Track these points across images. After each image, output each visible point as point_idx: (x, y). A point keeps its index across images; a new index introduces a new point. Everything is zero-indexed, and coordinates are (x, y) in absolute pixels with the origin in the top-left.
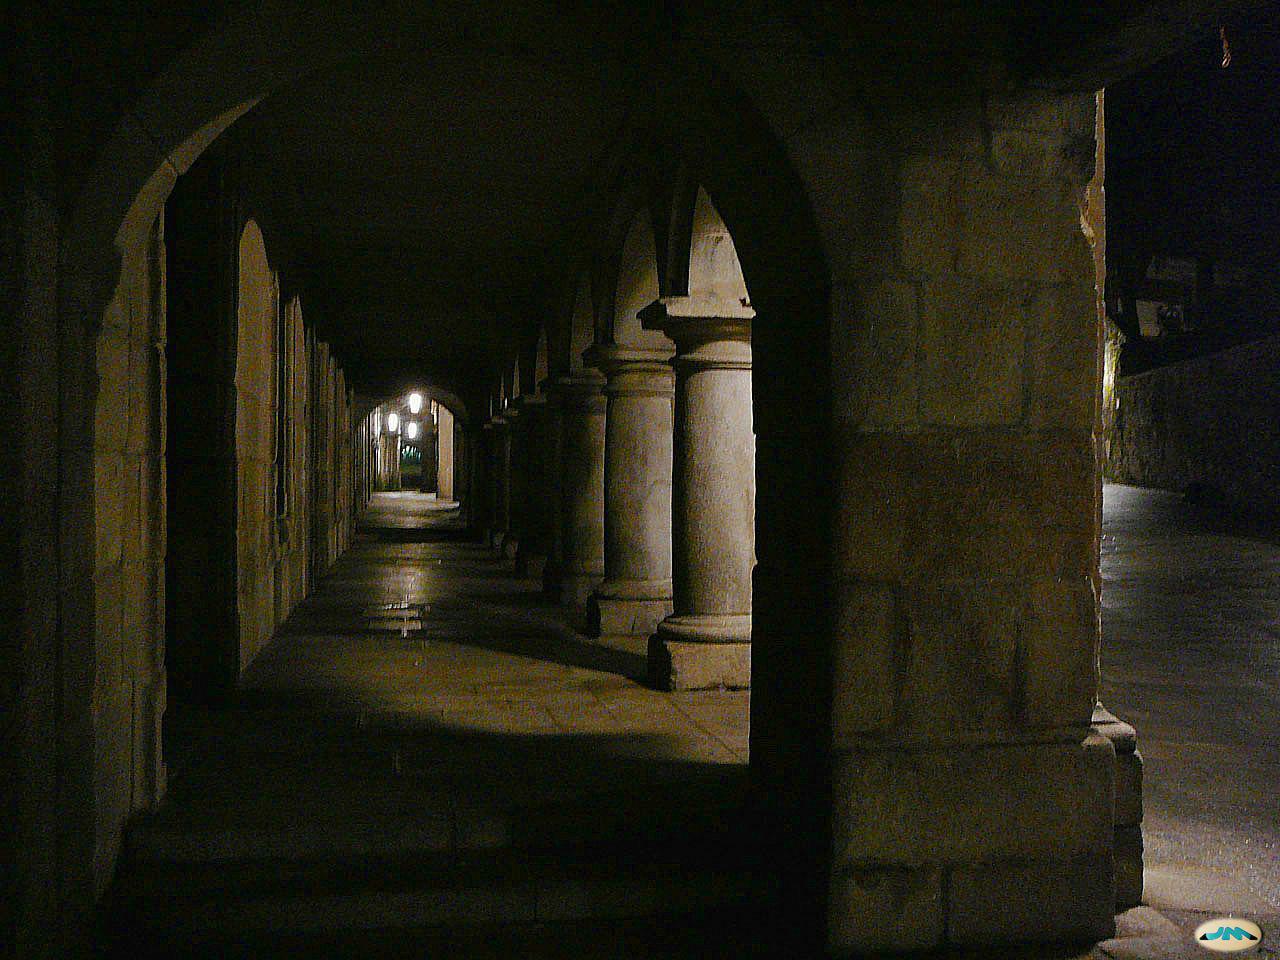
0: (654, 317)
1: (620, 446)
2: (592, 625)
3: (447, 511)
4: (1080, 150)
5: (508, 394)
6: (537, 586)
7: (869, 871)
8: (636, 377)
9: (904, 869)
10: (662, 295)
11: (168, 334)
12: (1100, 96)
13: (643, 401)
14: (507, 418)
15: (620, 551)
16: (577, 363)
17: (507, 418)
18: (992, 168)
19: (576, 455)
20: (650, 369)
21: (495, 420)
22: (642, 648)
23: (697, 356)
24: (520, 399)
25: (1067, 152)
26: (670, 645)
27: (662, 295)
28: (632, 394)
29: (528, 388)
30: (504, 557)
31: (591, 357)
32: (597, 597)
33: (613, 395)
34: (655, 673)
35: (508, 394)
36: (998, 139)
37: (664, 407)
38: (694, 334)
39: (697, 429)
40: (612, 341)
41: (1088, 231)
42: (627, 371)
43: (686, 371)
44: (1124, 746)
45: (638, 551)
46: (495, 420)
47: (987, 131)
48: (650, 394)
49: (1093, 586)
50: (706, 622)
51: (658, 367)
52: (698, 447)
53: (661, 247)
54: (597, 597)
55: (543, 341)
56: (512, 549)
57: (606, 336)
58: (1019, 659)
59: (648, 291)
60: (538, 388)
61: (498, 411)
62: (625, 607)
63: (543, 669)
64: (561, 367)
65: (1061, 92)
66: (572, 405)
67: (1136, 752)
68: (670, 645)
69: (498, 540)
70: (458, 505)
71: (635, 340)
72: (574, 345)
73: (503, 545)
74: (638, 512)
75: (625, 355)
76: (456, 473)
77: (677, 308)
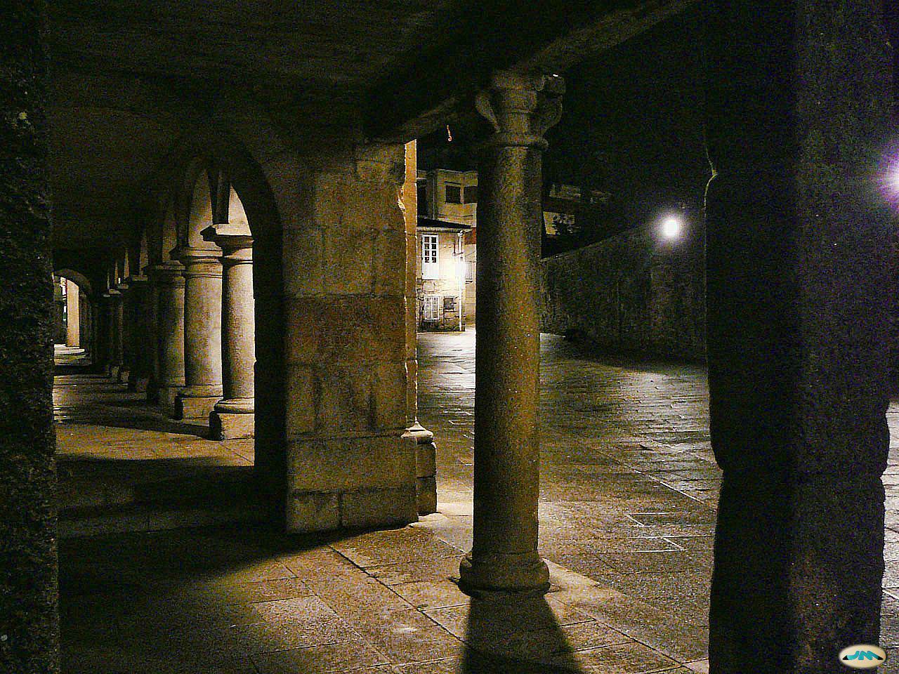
0: (209, 234)
1: (192, 306)
2: (178, 413)
3: (77, 354)
4: (399, 170)
5: (121, 275)
6: (143, 396)
7: (305, 495)
8: (201, 267)
9: (321, 494)
10: (214, 223)
11: (428, 227)
12: (411, 148)
13: (203, 280)
14: (120, 290)
15: (193, 370)
16: (166, 256)
17: (120, 290)
18: (357, 178)
19: (166, 311)
20: (209, 262)
21: (112, 291)
22: (207, 423)
23: (235, 256)
24: (130, 278)
25: (392, 171)
26: (221, 415)
27: (214, 223)
28: (203, 276)
29: (134, 270)
30: (120, 381)
31: (175, 254)
32: (180, 396)
33: (188, 277)
34: (214, 431)
35: (121, 275)
36: (361, 164)
37: (218, 283)
38: (229, 244)
39: (234, 296)
40: (188, 245)
41: (401, 206)
42: (197, 263)
43: (228, 265)
44: (425, 442)
45: (207, 371)
46: (112, 291)
47: (355, 161)
48: (211, 276)
49: (406, 367)
50: (241, 402)
51: (213, 260)
52: (235, 307)
53: (213, 195)
54: (180, 396)
55: (144, 241)
56: (125, 376)
57: (184, 243)
58: (372, 402)
59: (206, 221)
60: (142, 273)
61: (114, 286)
62: (197, 401)
63: (147, 434)
64: (156, 258)
65: (390, 144)
66: (164, 282)
67: (433, 443)
68: (221, 415)
69: (115, 371)
70: (83, 350)
71: (201, 248)
72: (165, 247)
73: (119, 374)
74: (205, 345)
75: (196, 254)
76: (81, 328)
77: (222, 230)
